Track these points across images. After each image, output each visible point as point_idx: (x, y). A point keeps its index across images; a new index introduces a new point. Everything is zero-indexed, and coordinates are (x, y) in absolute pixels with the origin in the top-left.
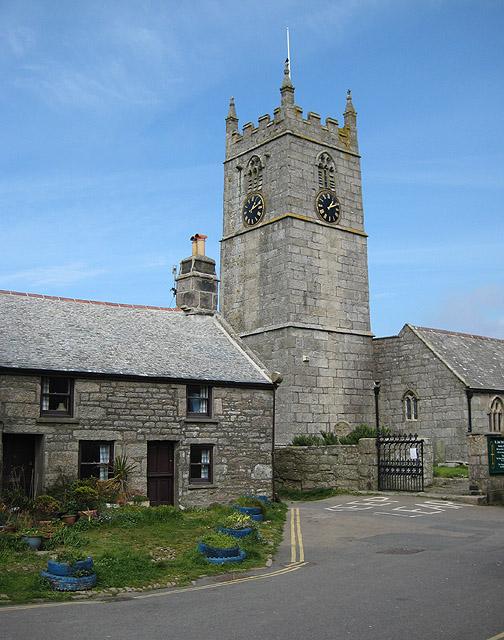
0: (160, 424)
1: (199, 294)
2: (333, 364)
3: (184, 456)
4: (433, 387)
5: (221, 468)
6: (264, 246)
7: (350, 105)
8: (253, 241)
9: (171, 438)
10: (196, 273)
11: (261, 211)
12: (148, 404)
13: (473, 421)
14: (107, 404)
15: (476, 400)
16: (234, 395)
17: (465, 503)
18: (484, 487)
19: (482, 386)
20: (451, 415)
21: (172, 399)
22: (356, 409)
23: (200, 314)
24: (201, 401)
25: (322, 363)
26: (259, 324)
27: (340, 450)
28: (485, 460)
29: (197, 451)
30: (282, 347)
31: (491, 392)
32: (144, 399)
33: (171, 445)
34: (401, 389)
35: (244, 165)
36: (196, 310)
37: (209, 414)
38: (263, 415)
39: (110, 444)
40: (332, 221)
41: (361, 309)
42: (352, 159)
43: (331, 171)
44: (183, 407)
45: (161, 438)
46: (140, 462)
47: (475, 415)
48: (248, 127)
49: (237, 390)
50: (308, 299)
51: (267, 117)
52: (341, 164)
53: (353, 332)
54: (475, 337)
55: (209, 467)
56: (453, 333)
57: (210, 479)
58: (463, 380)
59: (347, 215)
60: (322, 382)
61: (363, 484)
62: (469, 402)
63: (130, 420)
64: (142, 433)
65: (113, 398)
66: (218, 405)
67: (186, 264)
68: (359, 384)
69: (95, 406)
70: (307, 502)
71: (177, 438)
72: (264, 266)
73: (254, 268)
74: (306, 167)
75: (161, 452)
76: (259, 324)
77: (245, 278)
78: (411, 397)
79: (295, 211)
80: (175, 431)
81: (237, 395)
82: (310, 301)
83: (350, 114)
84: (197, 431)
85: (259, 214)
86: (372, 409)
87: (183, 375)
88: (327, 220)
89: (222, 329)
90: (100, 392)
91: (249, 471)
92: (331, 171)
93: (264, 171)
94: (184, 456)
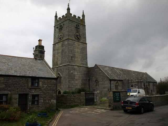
0: (23, 89)
1: (39, 54)
2: (79, 74)
3: (30, 98)
4: (102, 79)
5: (41, 101)
6: (63, 45)
7: (83, 14)
8: (60, 45)
9: (26, 93)
10: (39, 49)
11: (62, 37)
12: (19, 83)
13: (111, 87)
14: (6, 83)
15: (112, 82)
16: (45, 81)
17: (107, 110)
18: (112, 105)
19: (113, 79)
20: (106, 86)
21: (27, 82)
22: (84, 84)
23: (39, 60)
24: (36, 82)
25: (76, 73)
26: (61, 64)
27: (76, 95)
28: (112, 98)
29: (34, 96)
30: (66, 69)
31: (115, 80)
32: (18, 82)
33: (26, 95)
34: (94, 79)
35: (58, 27)
36: (38, 59)
37: (38, 86)
38: (54, 86)
39: (7, 95)
40: (79, 40)
41: (85, 61)
42: (84, 26)
43: (79, 28)
44: (30, 84)
45: (23, 93)
46: (16, 100)
47: (112, 86)
48: (60, 18)
49: (46, 80)
50: (73, 58)
51: (64, 16)
52: (81, 27)
53: (83, 66)
54: (112, 67)
55: (38, 101)
56: (107, 66)
57: (38, 104)
58: (109, 77)
59: (82, 39)
60: (76, 78)
61: (82, 104)
62: (110, 82)
63: (13, 88)
64: (17, 92)
65: (8, 82)
66: (41, 84)
67: (36, 47)
68: (85, 78)
69: (2, 84)
70: (66, 109)
71: (28, 93)
72: (63, 50)
73: (60, 51)
74: (73, 27)
75: (23, 97)
76: (61, 64)
77: (58, 53)
78: (97, 81)
79: (70, 38)
80: (28, 91)
81: (46, 81)
82: (73, 59)
83: (83, 16)
84: (34, 91)
85: (61, 38)
86: (88, 84)
87: (30, 75)
88: (77, 40)
89: (45, 64)
90: (4, 80)
91: (49, 101)
92: (79, 28)
93: (63, 28)
94: (30, 98)
